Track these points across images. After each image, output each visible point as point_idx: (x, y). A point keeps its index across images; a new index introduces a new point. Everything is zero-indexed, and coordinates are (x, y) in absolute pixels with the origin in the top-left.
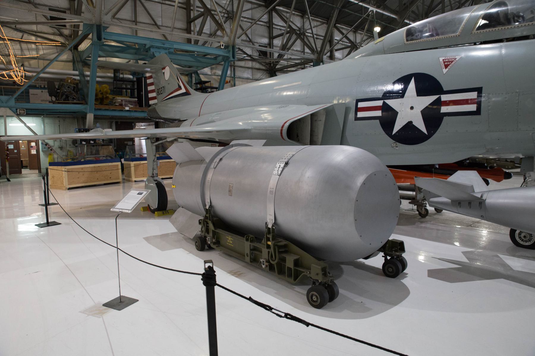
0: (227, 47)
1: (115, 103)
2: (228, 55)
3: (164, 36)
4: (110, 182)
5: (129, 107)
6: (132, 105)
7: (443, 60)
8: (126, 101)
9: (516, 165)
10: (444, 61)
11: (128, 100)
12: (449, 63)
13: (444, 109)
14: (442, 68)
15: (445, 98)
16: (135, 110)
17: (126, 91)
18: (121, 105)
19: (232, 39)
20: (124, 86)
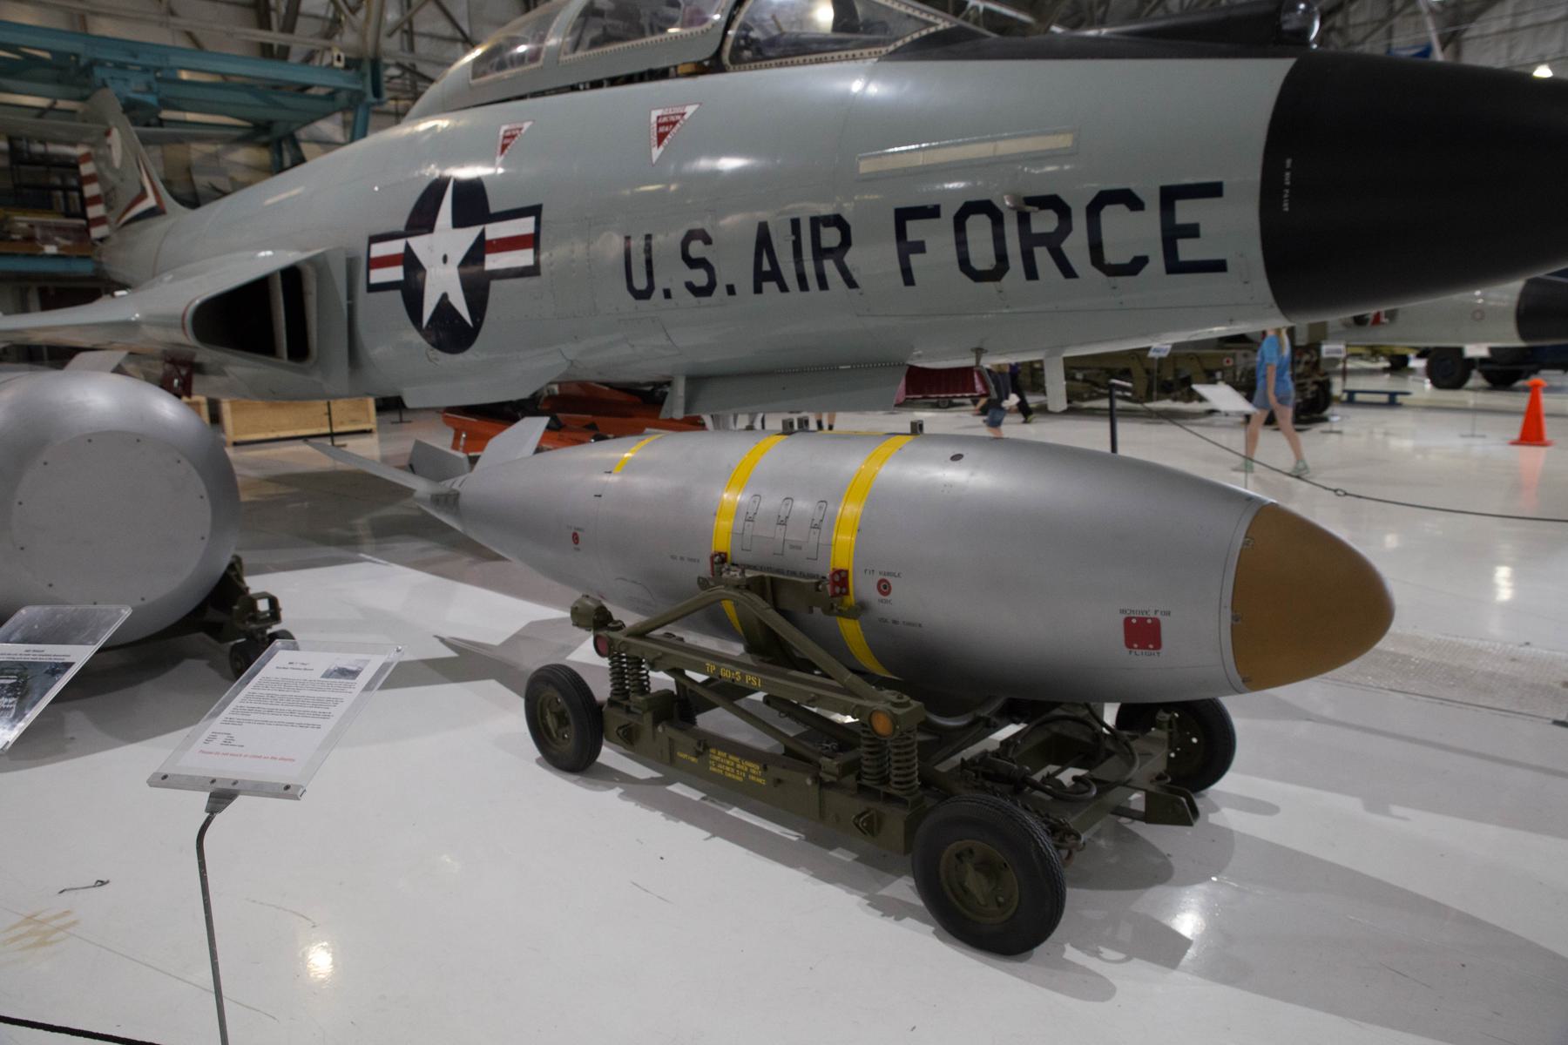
0: (352, 64)
1: (9, 232)
2: (358, 87)
3: (190, 35)
4: (1050, 440)
5: (56, 244)
6: (67, 238)
7: (658, 118)
8: (45, 226)
9: (1129, 385)
10: (660, 121)
11: (55, 223)
12: (667, 129)
13: (494, 262)
14: (650, 144)
15: (495, 231)
16: (80, 254)
17: (66, 198)
18: (30, 239)
19: (370, 39)
20: (58, 181)
